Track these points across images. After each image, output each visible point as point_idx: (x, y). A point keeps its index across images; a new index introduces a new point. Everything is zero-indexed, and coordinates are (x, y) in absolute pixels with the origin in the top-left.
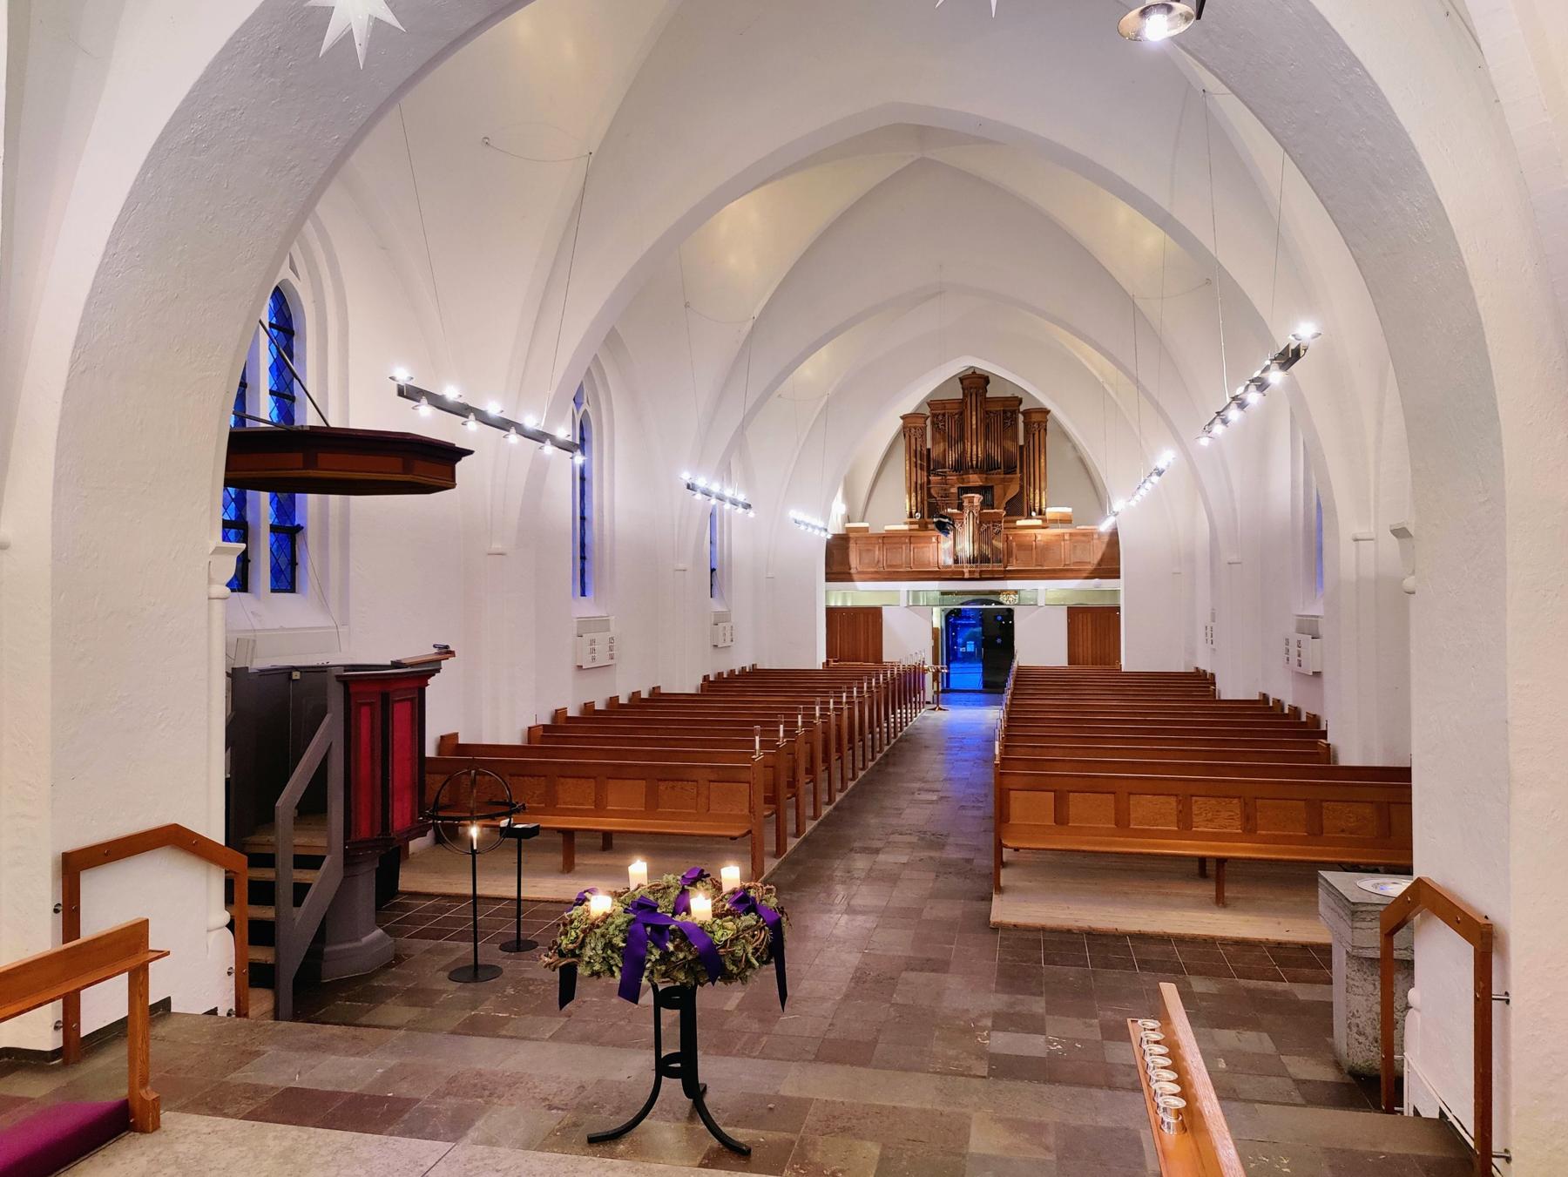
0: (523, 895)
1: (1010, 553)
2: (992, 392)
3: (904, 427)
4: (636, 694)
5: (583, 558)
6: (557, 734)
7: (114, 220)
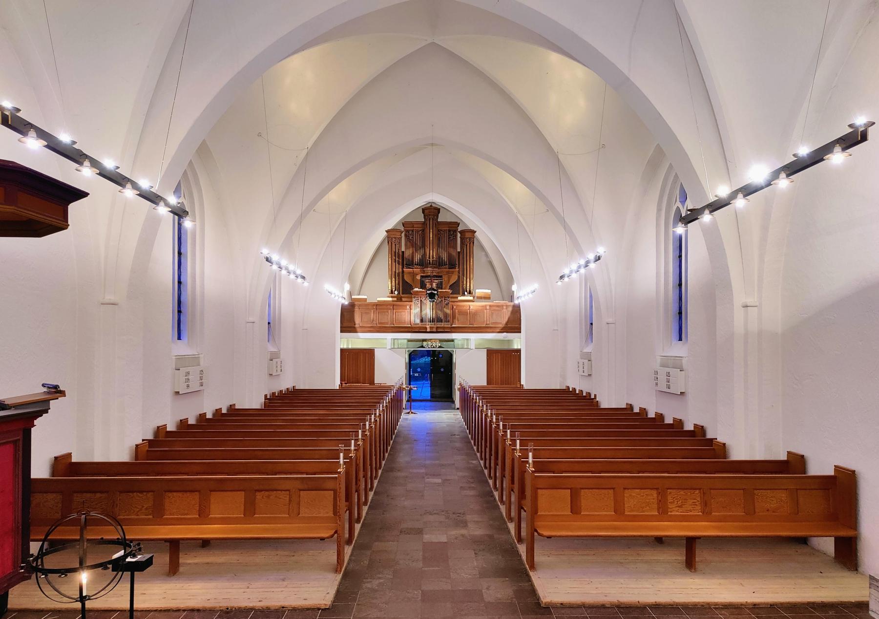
1: (454, 317)
3: (388, 237)
5: (179, 312)
6: (160, 448)
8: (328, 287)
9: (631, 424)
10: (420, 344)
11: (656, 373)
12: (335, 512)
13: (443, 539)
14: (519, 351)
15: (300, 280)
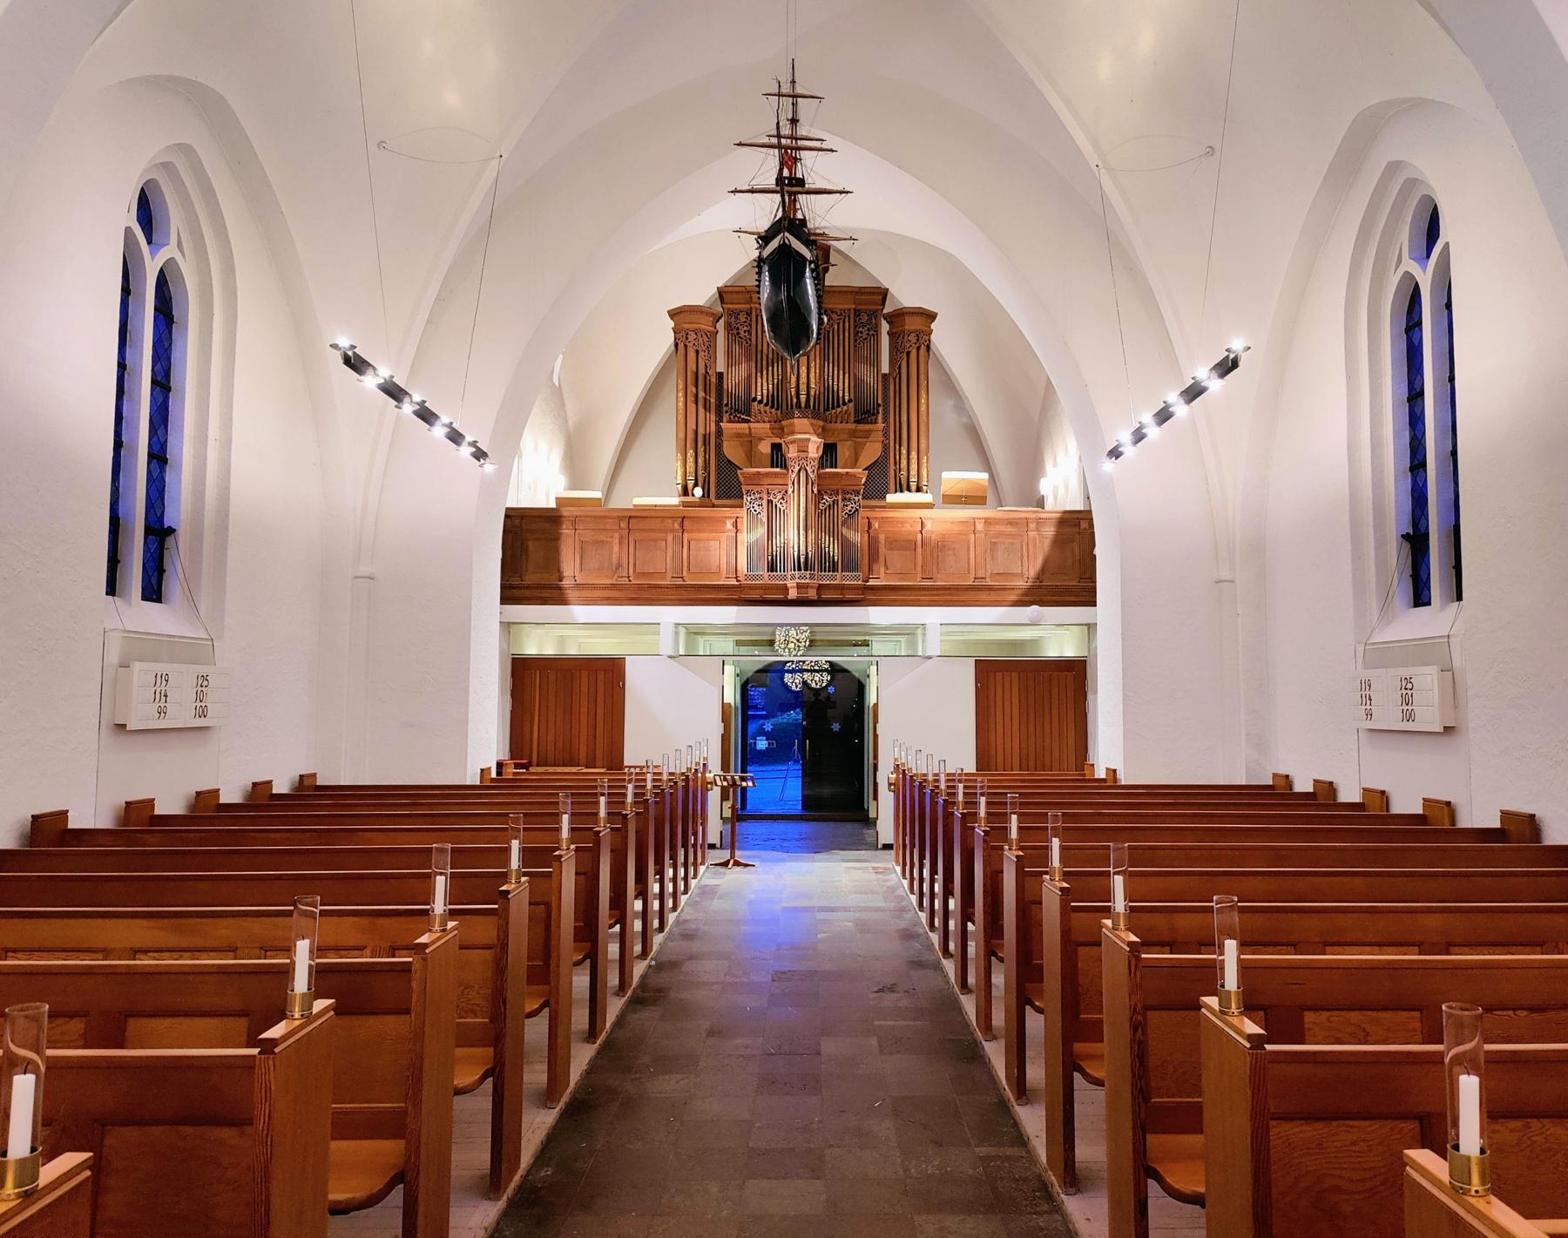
1: (873, 555)
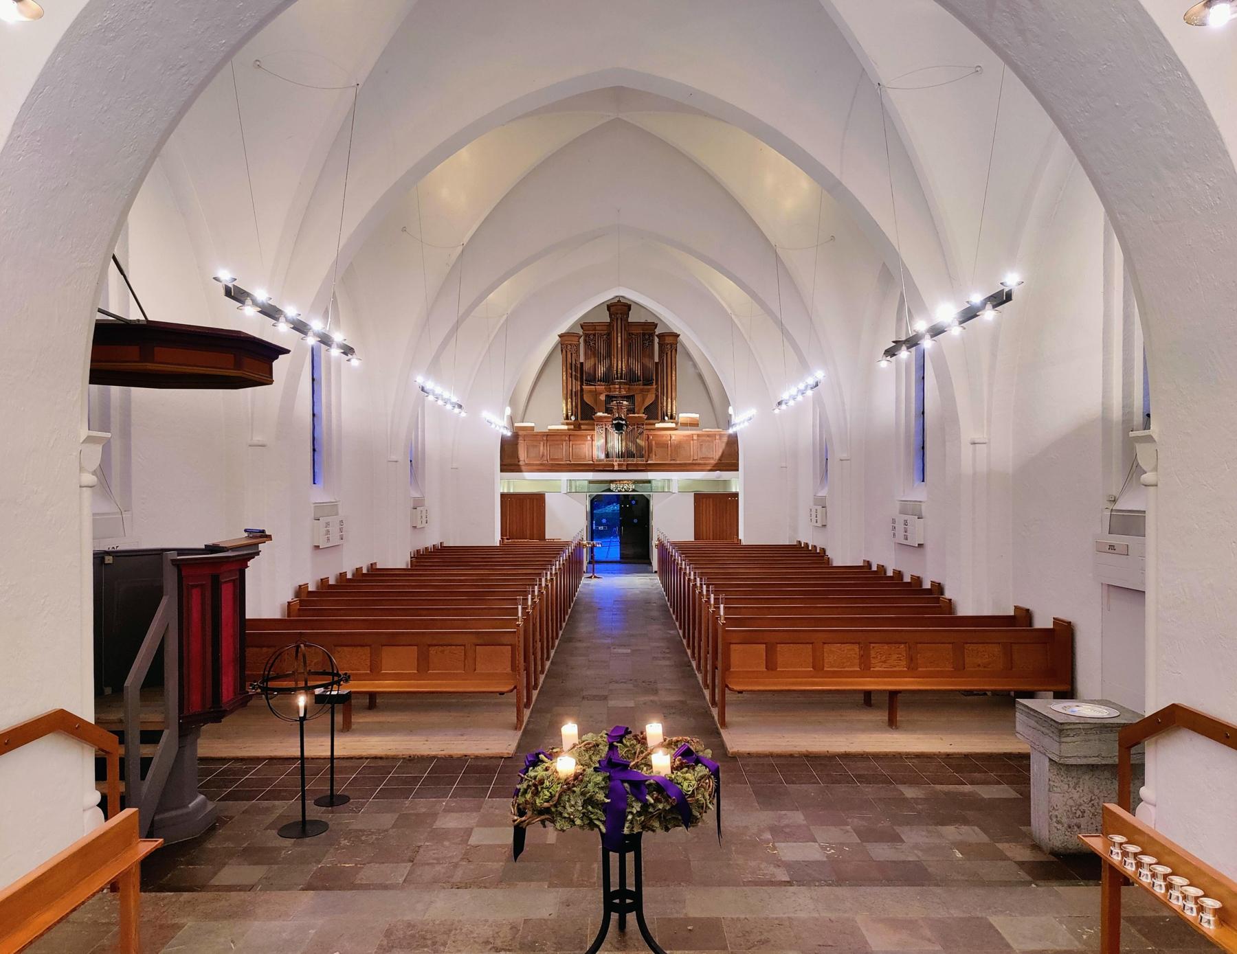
0: (306, 754)
2: (633, 317)
4: (359, 570)
7: (21, 100)
8: (486, 415)
9: (869, 584)
10: (605, 486)
11: (894, 521)
12: (514, 667)
13: (632, 704)
14: (736, 495)
15: (457, 410)
